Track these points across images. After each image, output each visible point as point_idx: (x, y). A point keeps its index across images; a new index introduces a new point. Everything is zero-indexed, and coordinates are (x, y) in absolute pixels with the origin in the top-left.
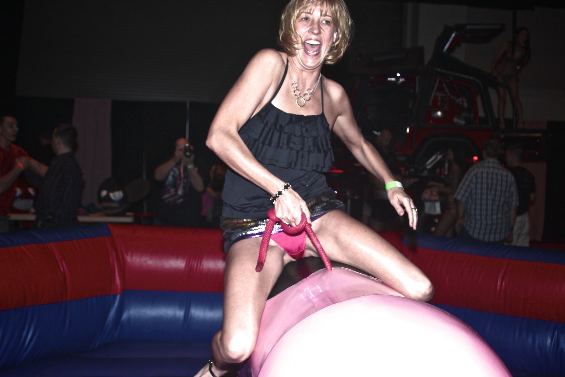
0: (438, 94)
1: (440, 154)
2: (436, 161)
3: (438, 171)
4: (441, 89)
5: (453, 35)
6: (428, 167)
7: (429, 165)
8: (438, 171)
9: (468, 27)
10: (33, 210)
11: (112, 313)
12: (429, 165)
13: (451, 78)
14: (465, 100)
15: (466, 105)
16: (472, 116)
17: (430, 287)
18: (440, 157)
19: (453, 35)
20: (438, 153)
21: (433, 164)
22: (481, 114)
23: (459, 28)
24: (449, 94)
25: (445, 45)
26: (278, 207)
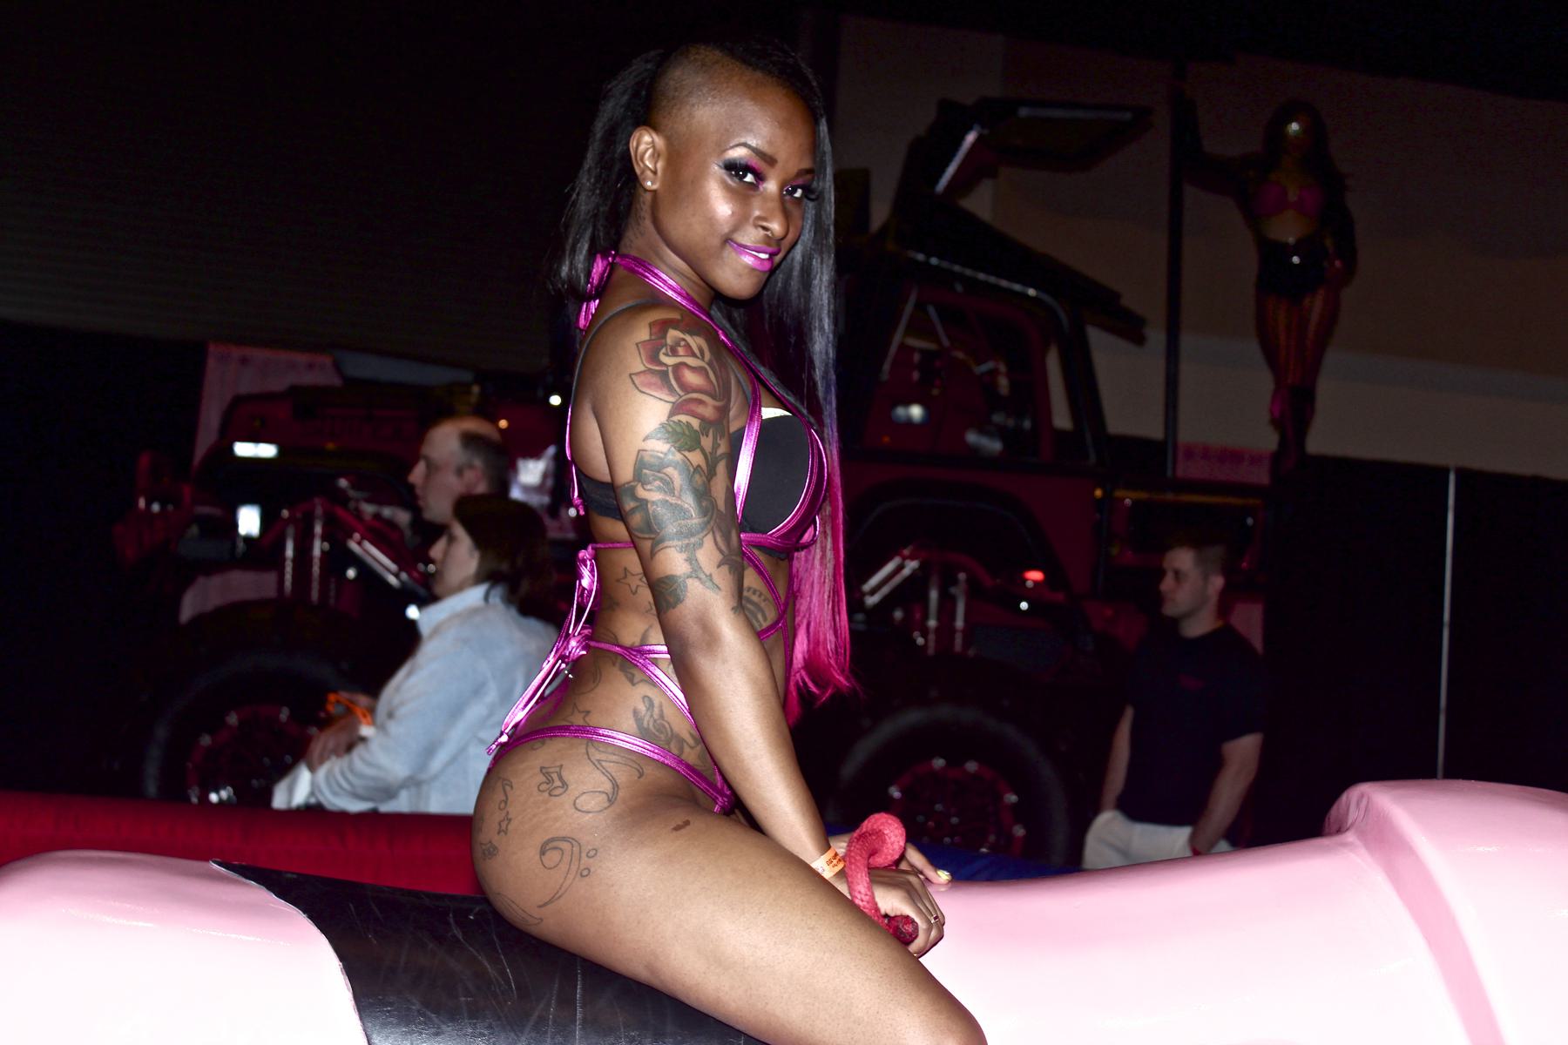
0: (913, 342)
1: (912, 558)
2: (897, 580)
3: (898, 614)
4: (919, 327)
5: (971, 138)
6: (871, 601)
7: (873, 592)
8: (898, 614)
9: (1024, 112)
10: (971, 652)
11: (670, 293)
12: (873, 592)
13: (959, 288)
14: (1002, 368)
15: (1003, 383)
16: (1027, 424)
17: (492, 851)
18: (912, 565)
19: (971, 138)
20: (906, 552)
21: (885, 590)
22: (1062, 419)
23: (988, 113)
24: (946, 342)
25: (947, 165)
26: (378, 767)
